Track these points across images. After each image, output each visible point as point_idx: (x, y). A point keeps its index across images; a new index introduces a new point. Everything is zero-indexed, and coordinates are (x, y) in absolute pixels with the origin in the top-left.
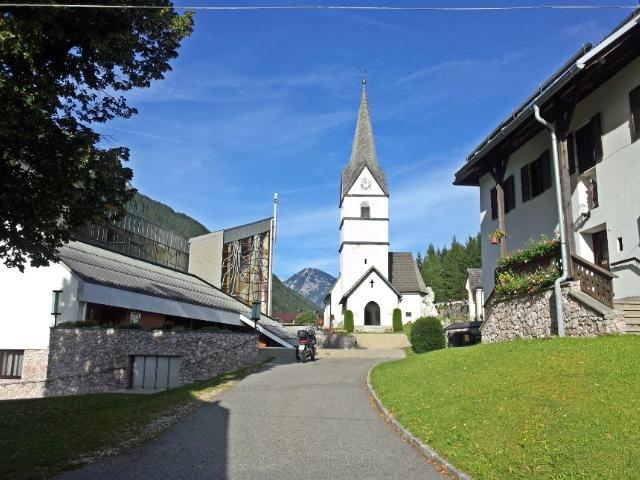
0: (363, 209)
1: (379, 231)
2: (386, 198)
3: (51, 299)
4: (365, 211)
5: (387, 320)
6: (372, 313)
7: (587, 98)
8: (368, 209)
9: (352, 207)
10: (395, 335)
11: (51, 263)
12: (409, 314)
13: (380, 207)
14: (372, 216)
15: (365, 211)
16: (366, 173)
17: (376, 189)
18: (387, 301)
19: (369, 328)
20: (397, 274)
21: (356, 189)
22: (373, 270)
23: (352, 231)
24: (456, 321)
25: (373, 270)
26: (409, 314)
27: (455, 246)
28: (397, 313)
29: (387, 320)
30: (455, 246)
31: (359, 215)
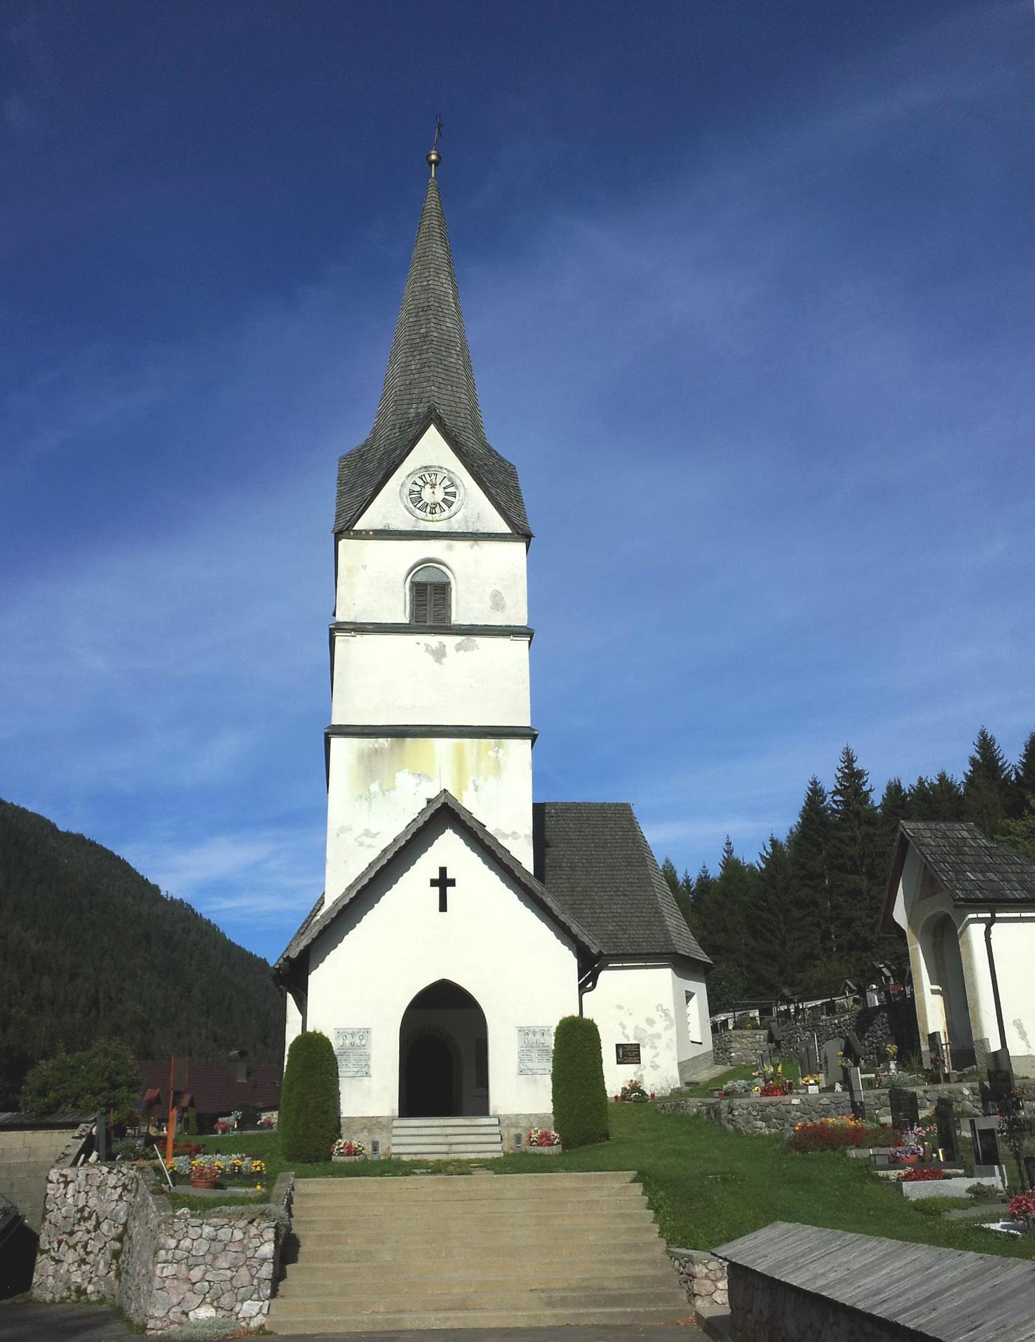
1: (494, 678)
2: (522, 546)
3: (372, 1072)
5: (519, 1089)
7: (422, 1327)
8: (443, 589)
9: (372, 577)
11: (649, 1093)
17: (477, 508)
18: (522, 976)
19: (428, 1136)
20: (583, 876)
21: (387, 508)
22: (444, 816)
23: (380, 677)
24: (965, 1123)
26: (628, 1054)
28: (576, 1045)
29: (519, 1089)
31: (403, 618)
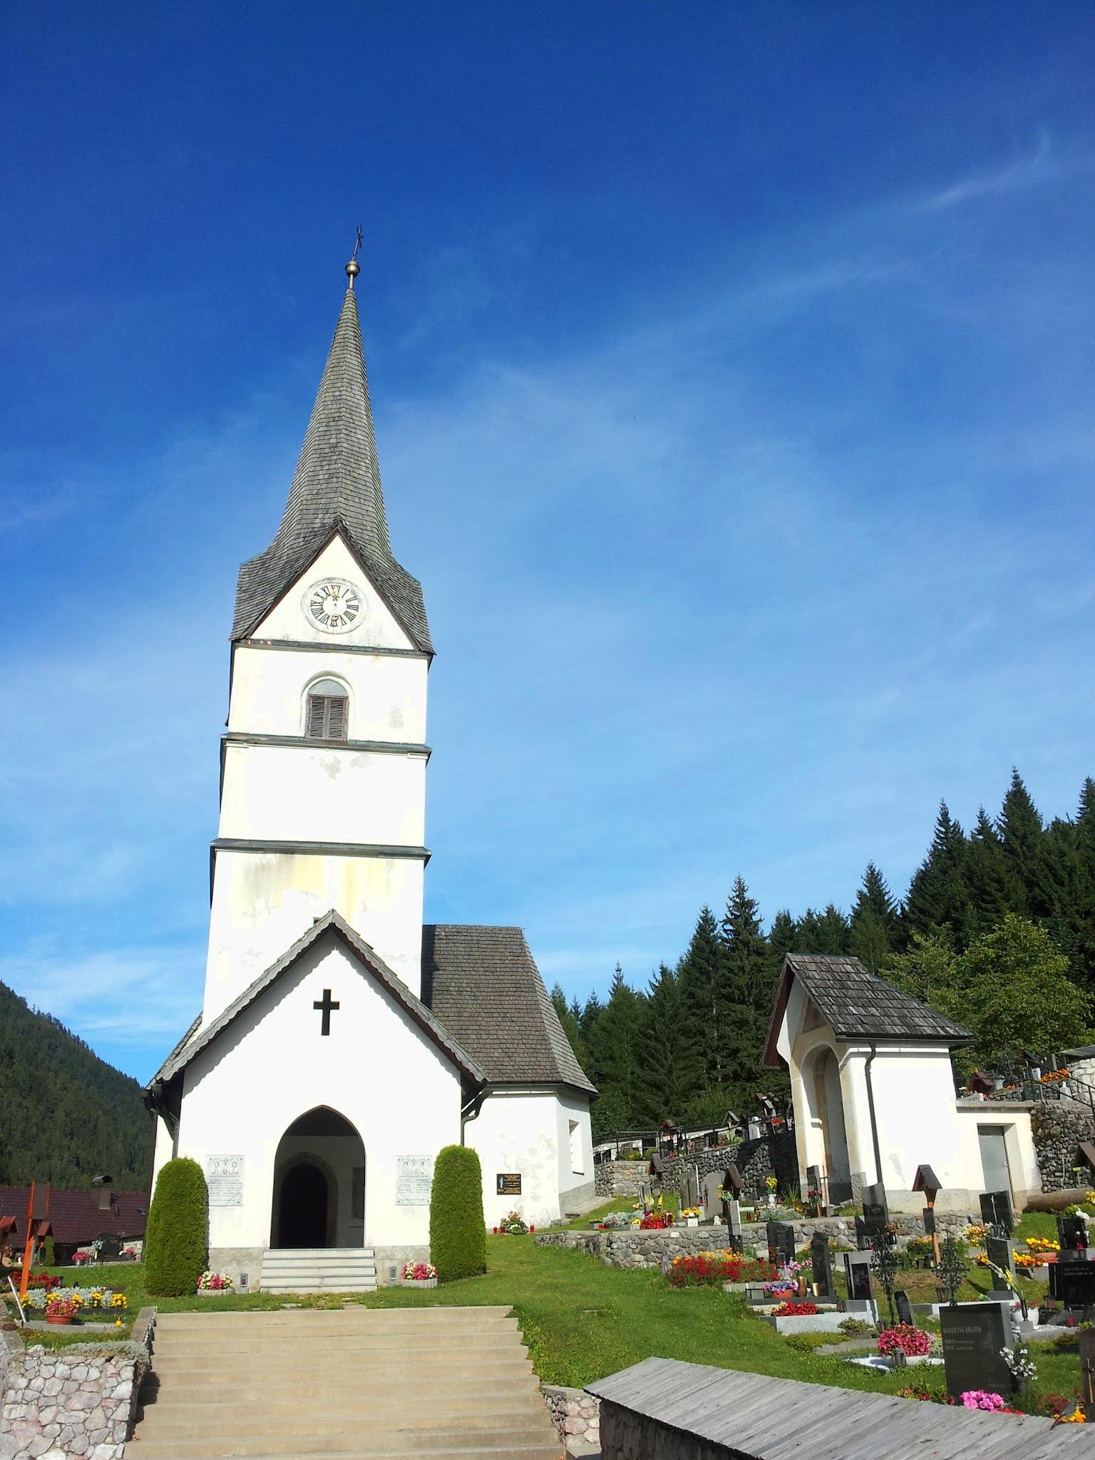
0: (316, 703)
4: (327, 717)
5: (396, 1219)
6: (317, 1183)
8: (340, 703)
9: (268, 690)
10: (438, 1315)
11: (528, 1225)
12: (510, 1184)
13: (391, 696)
14: (357, 729)
15: (327, 717)
16: (336, 560)
18: (402, 1104)
19: (303, 1268)
20: (465, 994)
21: (289, 618)
22: (332, 936)
25: (332, 936)
26: (510, 1184)
27: (621, 993)
28: (456, 1177)
29: (396, 1219)
30: (621, 993)
31: (299, 731)
